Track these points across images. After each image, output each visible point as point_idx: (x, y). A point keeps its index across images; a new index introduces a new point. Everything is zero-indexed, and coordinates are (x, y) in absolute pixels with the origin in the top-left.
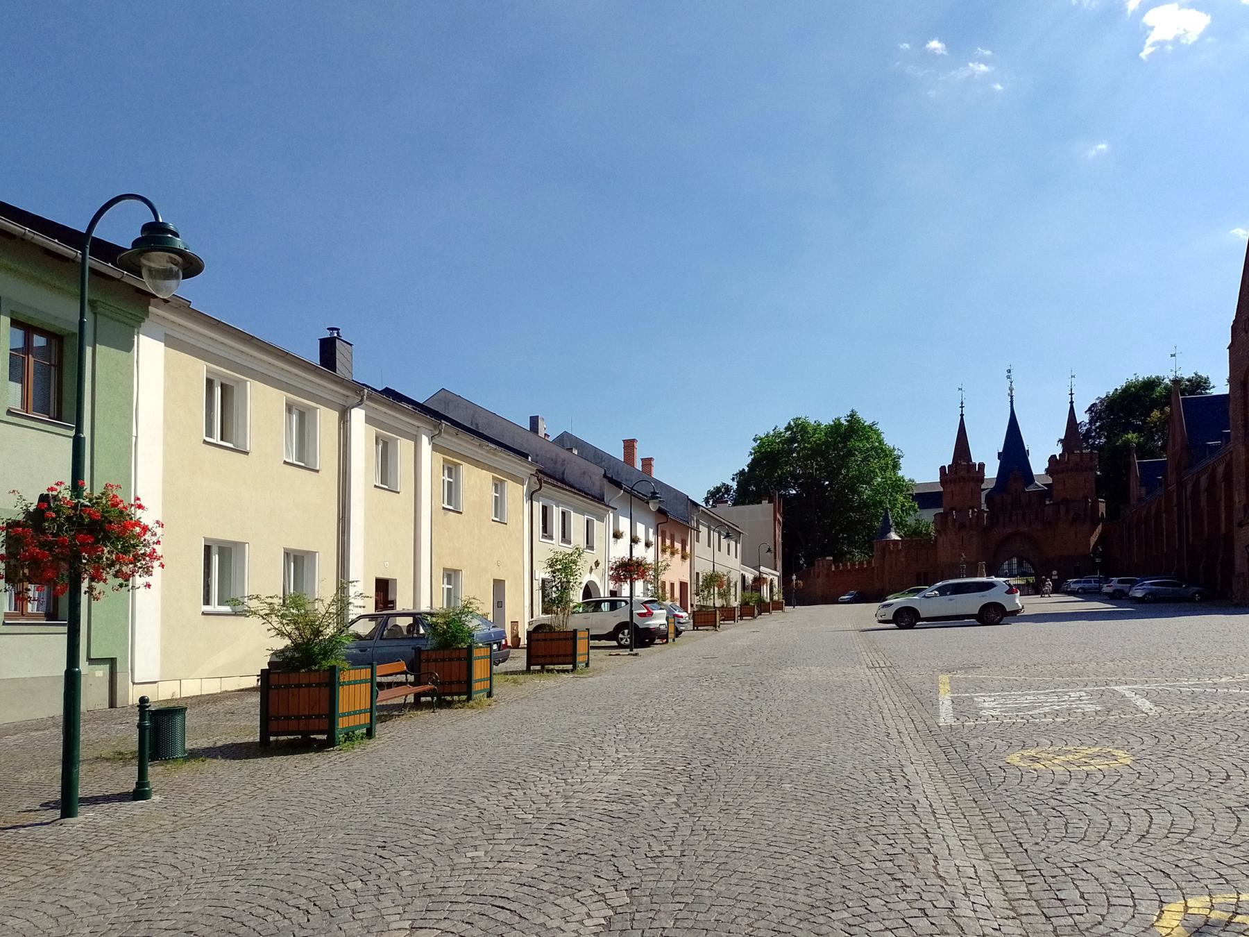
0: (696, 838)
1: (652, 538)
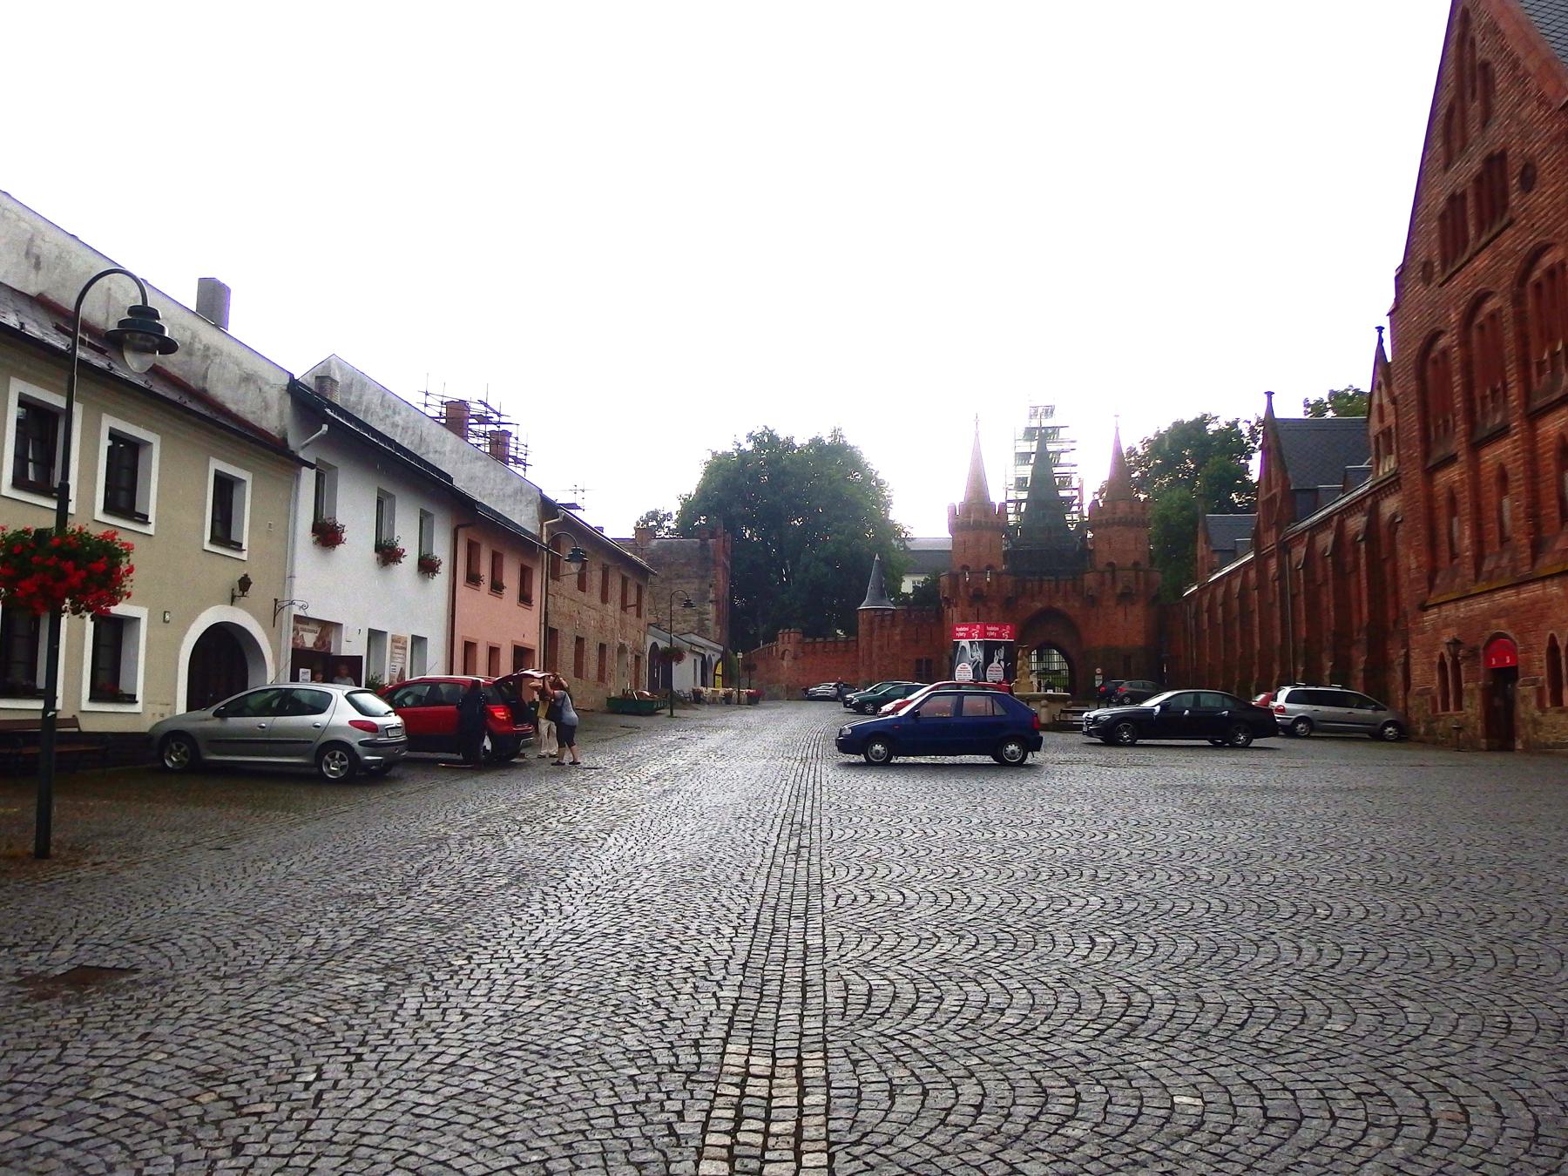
0: (68, 1022)
1: (441, 549)
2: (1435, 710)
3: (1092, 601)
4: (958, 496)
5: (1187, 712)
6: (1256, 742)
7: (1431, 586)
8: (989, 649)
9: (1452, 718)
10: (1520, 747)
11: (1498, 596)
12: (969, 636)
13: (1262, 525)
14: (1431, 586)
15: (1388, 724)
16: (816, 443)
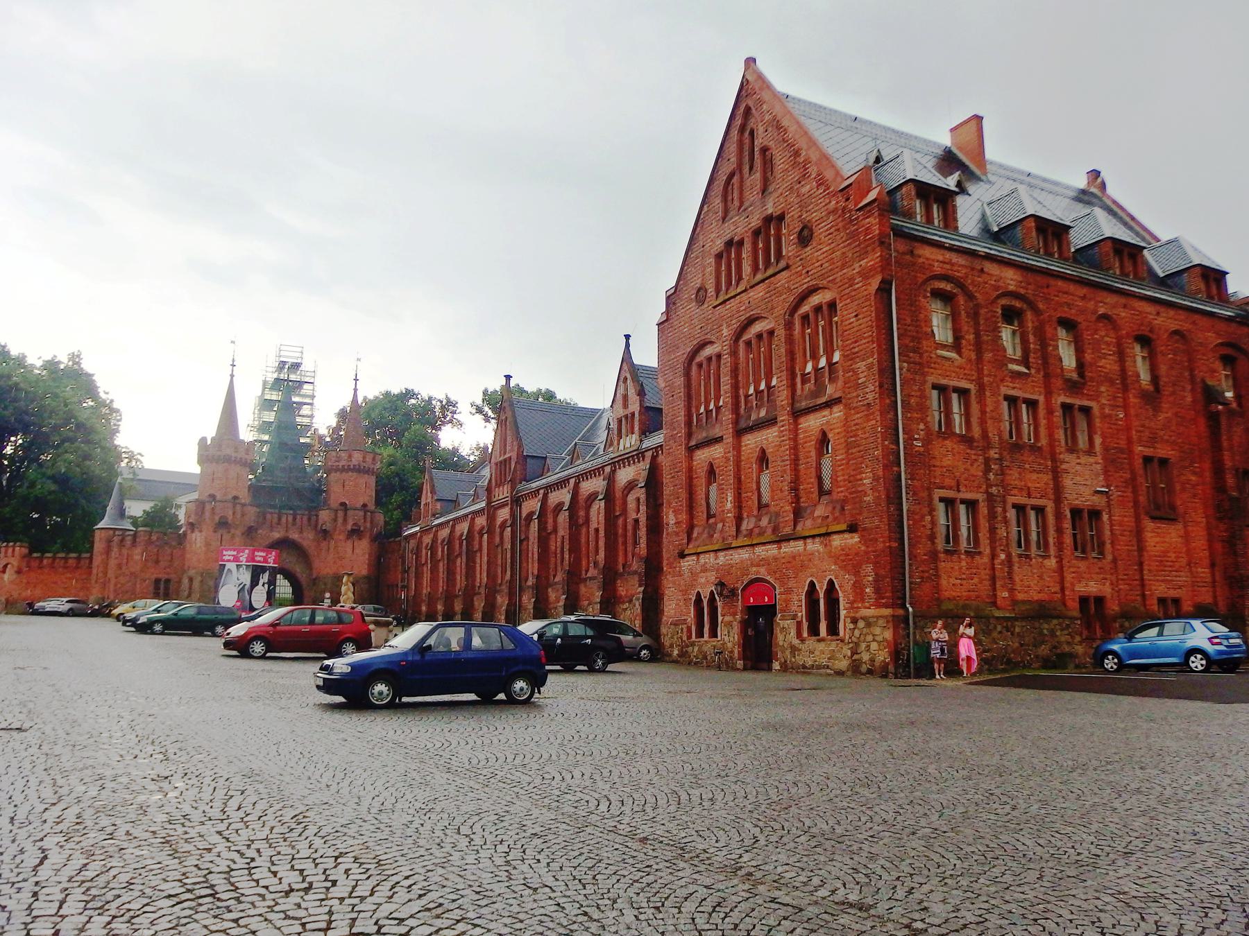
2: (689, 637)
3: (325, 534)
4: (210, 431)
5: (559, 641)
6: (610, 667)
7: (689, 539)
8: (256, 573)
9: (707, 644)
10: (778, 668)
11: (758, 550)
12: (236, 559)
13: (493, 481)
14: (689, 539)
15: (644, 647)
16: (51, 366)
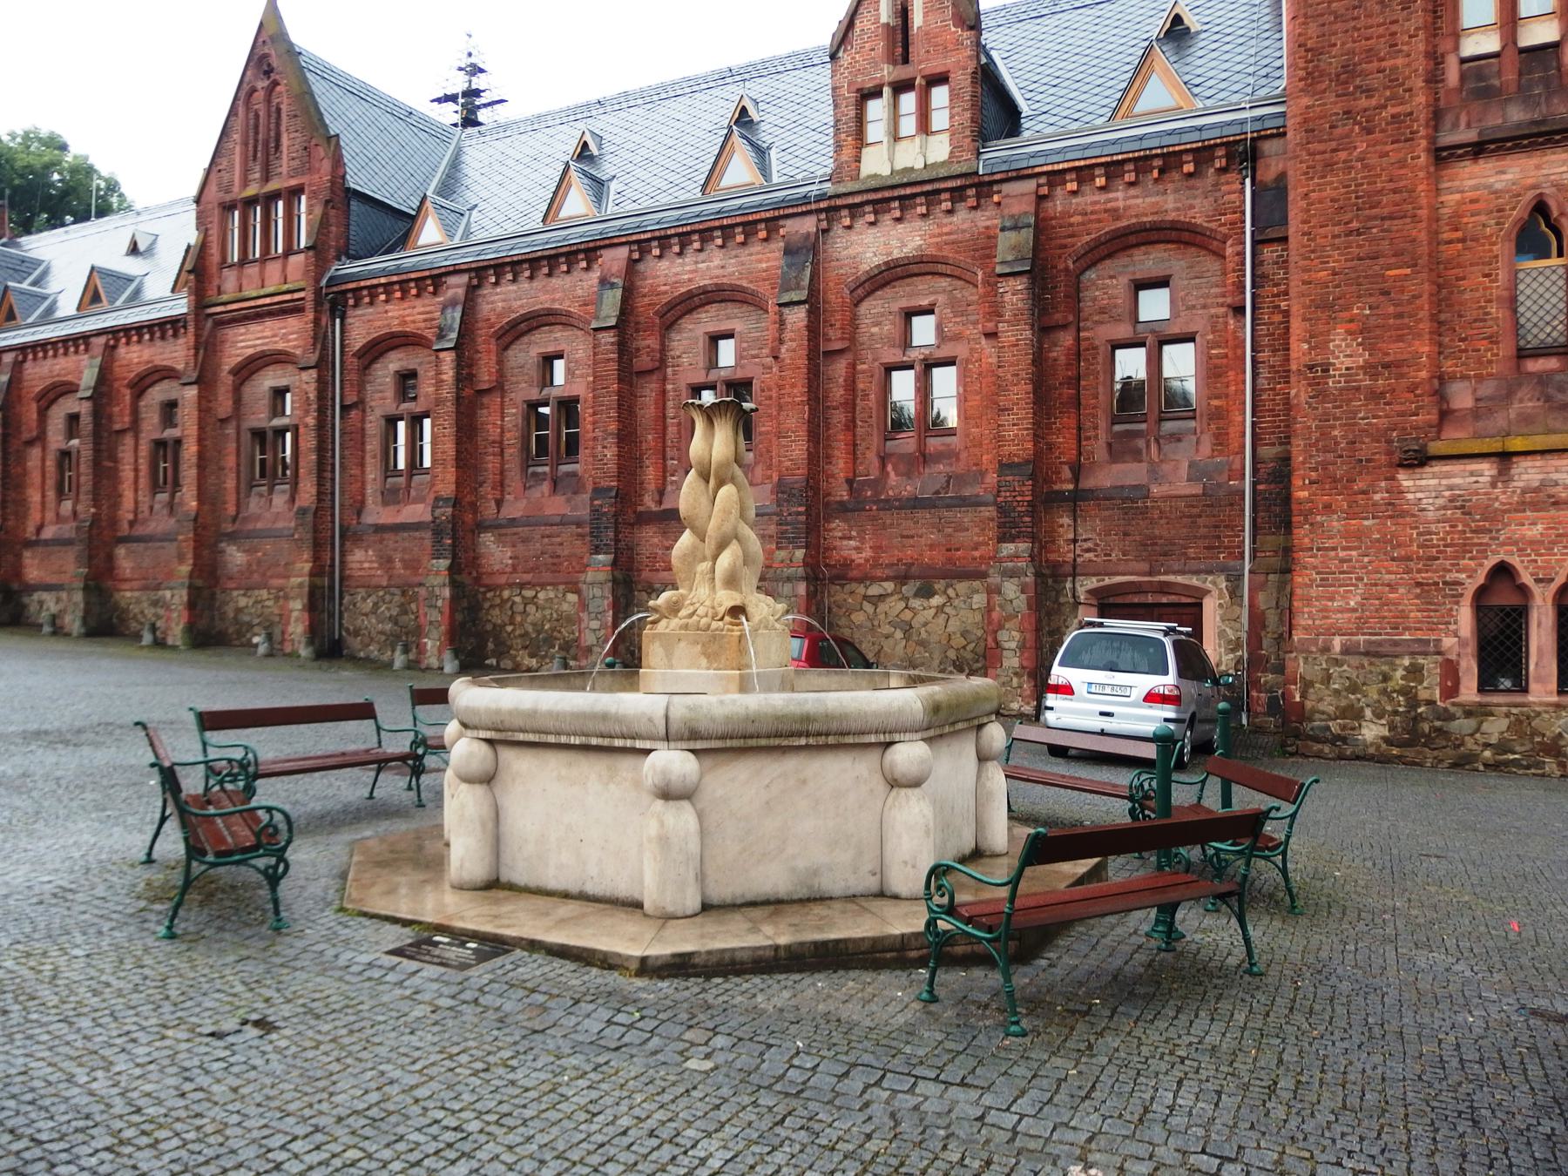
2: (1451, 691)
